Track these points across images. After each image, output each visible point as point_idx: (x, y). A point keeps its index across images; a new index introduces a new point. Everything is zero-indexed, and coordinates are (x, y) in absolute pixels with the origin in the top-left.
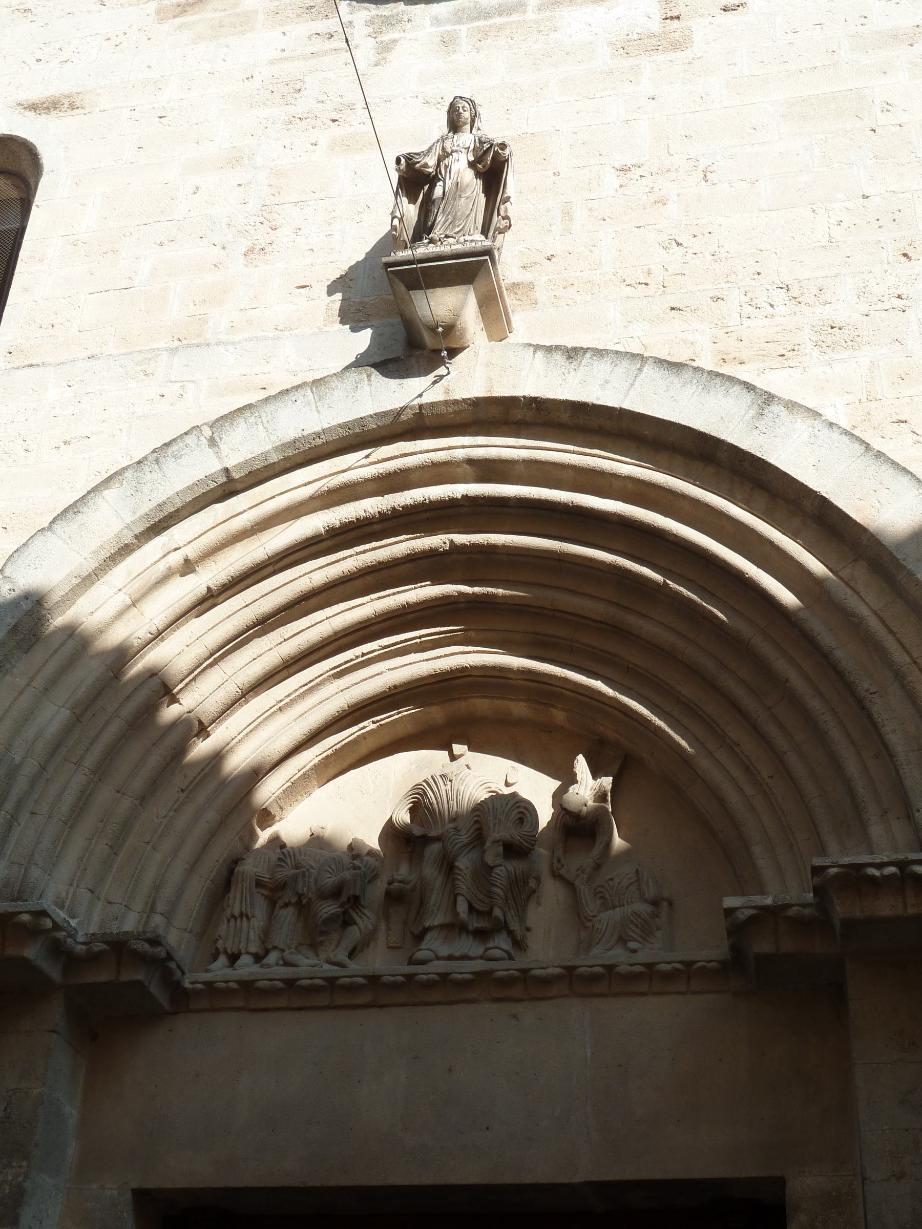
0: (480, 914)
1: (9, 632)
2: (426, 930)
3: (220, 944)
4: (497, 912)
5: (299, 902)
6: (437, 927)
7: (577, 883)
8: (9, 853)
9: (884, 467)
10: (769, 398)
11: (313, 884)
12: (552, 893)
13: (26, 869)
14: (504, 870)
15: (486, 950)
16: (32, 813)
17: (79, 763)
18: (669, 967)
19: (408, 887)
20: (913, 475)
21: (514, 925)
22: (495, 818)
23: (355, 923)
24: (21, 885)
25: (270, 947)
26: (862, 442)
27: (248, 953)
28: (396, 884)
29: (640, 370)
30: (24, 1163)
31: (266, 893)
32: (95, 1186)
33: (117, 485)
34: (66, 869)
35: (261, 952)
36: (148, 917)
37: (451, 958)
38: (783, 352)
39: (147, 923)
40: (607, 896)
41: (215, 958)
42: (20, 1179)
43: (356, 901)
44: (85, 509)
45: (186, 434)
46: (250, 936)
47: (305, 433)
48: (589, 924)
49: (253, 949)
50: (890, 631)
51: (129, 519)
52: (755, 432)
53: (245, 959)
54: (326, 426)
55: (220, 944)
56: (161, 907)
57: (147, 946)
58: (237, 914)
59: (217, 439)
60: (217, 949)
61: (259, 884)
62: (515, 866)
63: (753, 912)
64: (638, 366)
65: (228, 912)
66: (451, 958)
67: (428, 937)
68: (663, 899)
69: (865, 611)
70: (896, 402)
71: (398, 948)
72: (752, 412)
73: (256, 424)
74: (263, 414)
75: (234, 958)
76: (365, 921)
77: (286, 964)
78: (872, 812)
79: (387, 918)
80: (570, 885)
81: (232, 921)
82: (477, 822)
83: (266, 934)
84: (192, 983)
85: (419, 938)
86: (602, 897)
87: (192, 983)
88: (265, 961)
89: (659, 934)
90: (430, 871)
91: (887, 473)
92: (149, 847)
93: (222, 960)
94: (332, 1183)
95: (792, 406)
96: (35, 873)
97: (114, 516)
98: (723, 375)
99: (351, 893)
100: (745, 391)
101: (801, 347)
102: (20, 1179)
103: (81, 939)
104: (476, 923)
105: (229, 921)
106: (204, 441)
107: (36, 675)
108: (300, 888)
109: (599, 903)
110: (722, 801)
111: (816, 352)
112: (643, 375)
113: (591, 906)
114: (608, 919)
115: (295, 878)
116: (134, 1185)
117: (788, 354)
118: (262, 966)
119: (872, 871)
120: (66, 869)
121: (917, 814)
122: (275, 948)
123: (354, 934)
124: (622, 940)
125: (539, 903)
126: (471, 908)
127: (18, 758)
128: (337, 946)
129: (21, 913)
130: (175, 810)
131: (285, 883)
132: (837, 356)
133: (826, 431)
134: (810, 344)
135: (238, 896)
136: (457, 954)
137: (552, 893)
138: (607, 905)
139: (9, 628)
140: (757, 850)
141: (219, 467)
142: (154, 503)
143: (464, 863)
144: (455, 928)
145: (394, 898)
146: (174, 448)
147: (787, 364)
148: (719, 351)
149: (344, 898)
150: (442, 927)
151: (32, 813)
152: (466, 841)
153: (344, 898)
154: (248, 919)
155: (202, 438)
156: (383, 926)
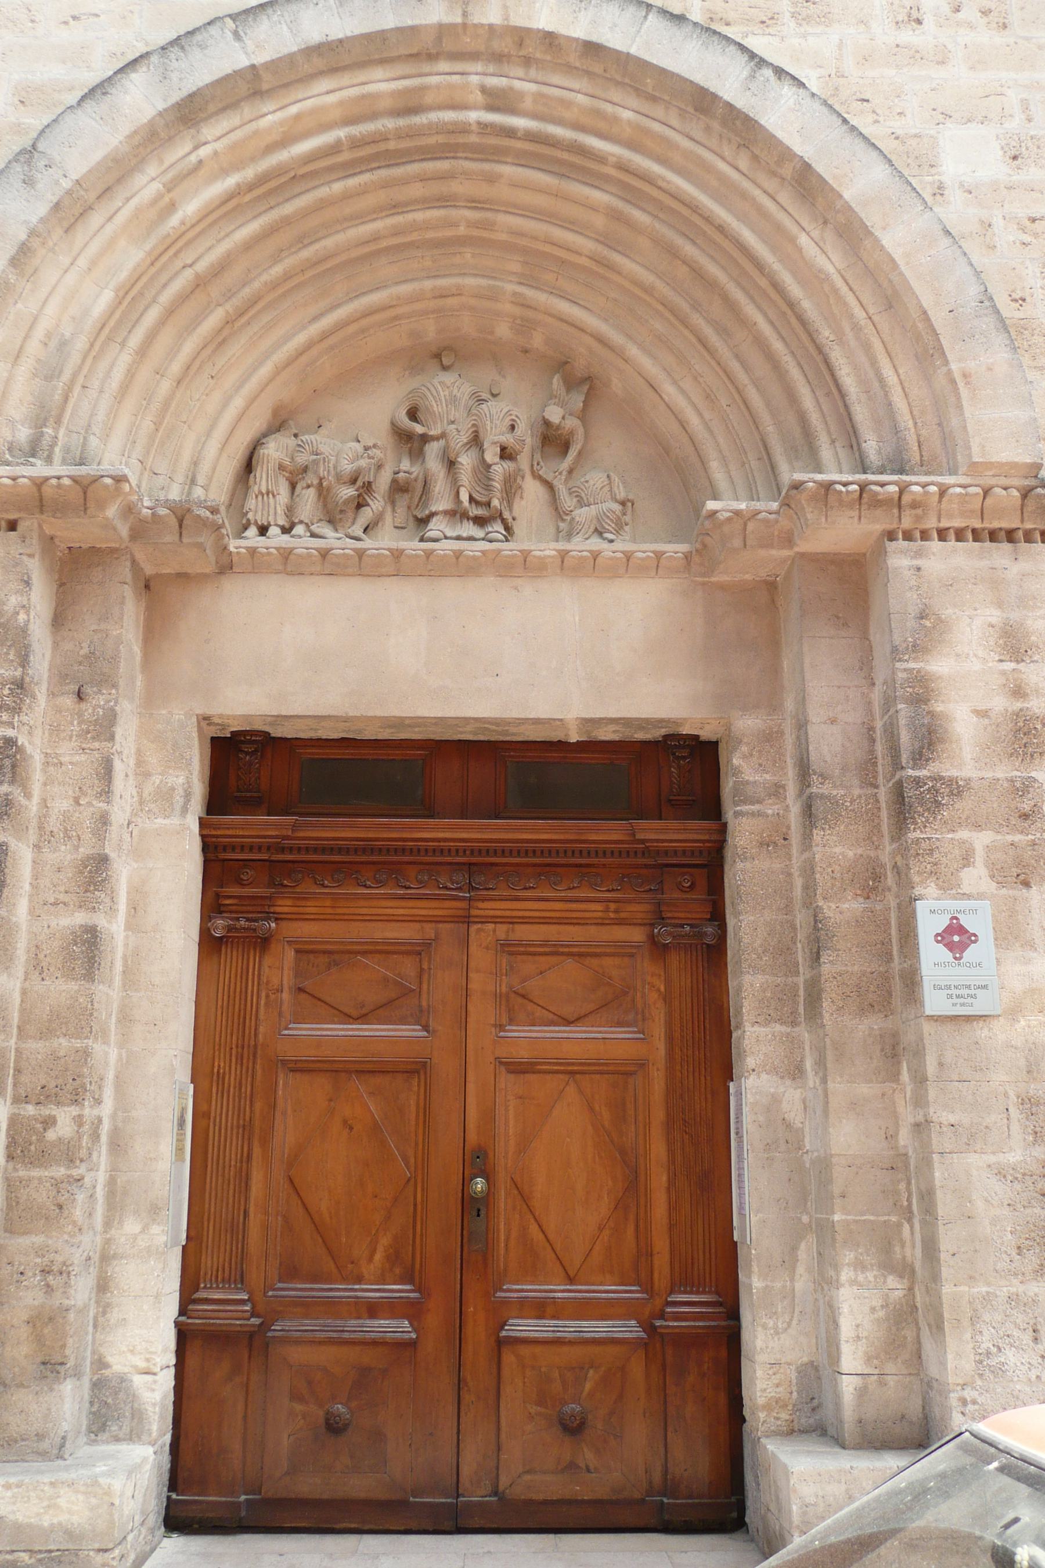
0: (478, 503)
1: (51, 209)
2: (432, 515)
3: (250, 516)
4: (495, 502)
5: (320, 484)
6: (442, 512)
7: (555, 483)
8: (66, 421)
9: (856, 141)
10: (761, 62)
11: (332, 469)
12: (532, 489)
13: (85, 438)
14: (500, 469)
15: (487, 534)
16: (84, 387)
17: (123, 344)
18: (644, 555)
19: (412, 476)
20: (881, 151)
21: (506, 515)
22: (491, 422)
23: (368, 505)
24: (82, 452)
25: (297, 521)
26: (839, 115)
27: (276, 525)
28: (401, 474)
29: (646, 17)
30: (114, 691)
31: (287, 475)
32: (164, 712)
33: (144, 69)
34: (116, 442)
35: (287, 526)
36: (190, 488)
37: (459, 538)
38: (764, 19)
39: (189, 494)
40: (583, 495)
41: (246, 528)
42: (112, 704)
43: (368, 487)
44: (113, 91)
45: (209, 24)
46: (276, 514)
47: (330, 39)
48: (568, 518)
49: (281, 522)
50: (851, 289)
51: (161, 106)
52: (748, 93)
53: (274, 531)
54: (349, 34)
55: (250, 516)
56: (201, 480)
57: (208, 513)
58: (264, 491)
59: (242, 34)
60: (248, 520)
61: (281, 467)
62: (508, 465)
63: (729, 514)
64: (644, 14)
65: (256, 489)
66: (459, 538)
67: (435, 519)
68: (629, 500)
69: (831, 270)
70: (861, 81)
71: (402, 528)
72: (745, 73)
73: (280, 23)
74: (286, 14)
75: (263, 530)
76: (376, 504)
77: (313, 535)
78: (823, 441)
79: (393, 503)
80: (549, 486)
81: (260, 498)
82: (474, 425)
83: (290, 510)
84: (237, 548)
85: (423, 522)
86: (577, 496)
87: (237, 548)
88: (293, 532)
89: (627, 528)
90: (433, 463)
91: (859, 145)
92: (186, 426)
93: (252, 531)
94: (370, 714)
95: (780, 72)
96: (94, 442)
97: (142, 100)
98: (719, 33)
99: (367, 479)
100: (739, 52)
101: (781, 16)
102: (112, 704)
103: (147, 503)
104: (475, 511)
105: (257, 497)
106: (229, 35)
107: (79, 254)
108: (322, 472)
109: (575, 500)
110: (683, 424)
111: (792, 24)
112: (648, 23)
113: (568, 502)
114: (583, 514)
115: (316, 462)
116: (199, 712)
117: (769, 22)
118: (292, 537)
119: (839, 487)
120: (116, 442)
121: (864, 445)
122: (301, 522)
123: (366, 515)
124: (599, 533)
125: (522, 498)
126: (472, 499)
127: (67, 335)
128: (353, 523)
129: (102, 476)
130: (207, 395)
131: (306, 467)
132: (810, 30)
133: (808, 99)
134: (788, 15)
135: (264, 476)
136: (465, 535)
137: (532, 489)
138: (581, 503)
139: (52, 205)
140: (714, 465)
141: (247, 63)
142: (184, 93)
143: (466, 461)
144: (457, 514)
145: (399, 488)
146: (198, 37)
147: (767, 31)
148: (708, 10)
149: (359, 483)
150: (446, 513)
151: (84, 387)
152: (465, 441)
153: (359, 483)
154: (274, 496)
155: (226, 31)
156: (389, 509)
